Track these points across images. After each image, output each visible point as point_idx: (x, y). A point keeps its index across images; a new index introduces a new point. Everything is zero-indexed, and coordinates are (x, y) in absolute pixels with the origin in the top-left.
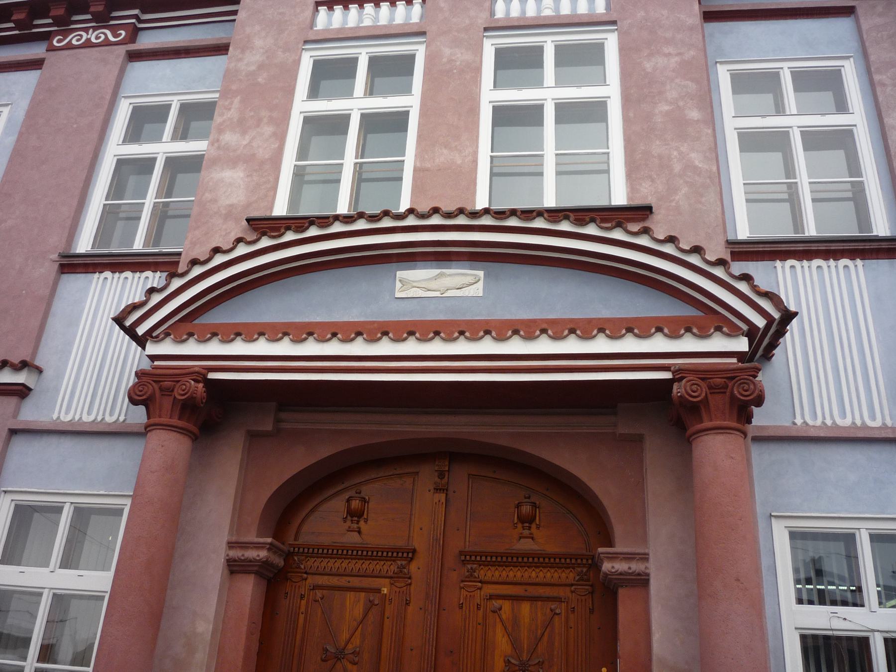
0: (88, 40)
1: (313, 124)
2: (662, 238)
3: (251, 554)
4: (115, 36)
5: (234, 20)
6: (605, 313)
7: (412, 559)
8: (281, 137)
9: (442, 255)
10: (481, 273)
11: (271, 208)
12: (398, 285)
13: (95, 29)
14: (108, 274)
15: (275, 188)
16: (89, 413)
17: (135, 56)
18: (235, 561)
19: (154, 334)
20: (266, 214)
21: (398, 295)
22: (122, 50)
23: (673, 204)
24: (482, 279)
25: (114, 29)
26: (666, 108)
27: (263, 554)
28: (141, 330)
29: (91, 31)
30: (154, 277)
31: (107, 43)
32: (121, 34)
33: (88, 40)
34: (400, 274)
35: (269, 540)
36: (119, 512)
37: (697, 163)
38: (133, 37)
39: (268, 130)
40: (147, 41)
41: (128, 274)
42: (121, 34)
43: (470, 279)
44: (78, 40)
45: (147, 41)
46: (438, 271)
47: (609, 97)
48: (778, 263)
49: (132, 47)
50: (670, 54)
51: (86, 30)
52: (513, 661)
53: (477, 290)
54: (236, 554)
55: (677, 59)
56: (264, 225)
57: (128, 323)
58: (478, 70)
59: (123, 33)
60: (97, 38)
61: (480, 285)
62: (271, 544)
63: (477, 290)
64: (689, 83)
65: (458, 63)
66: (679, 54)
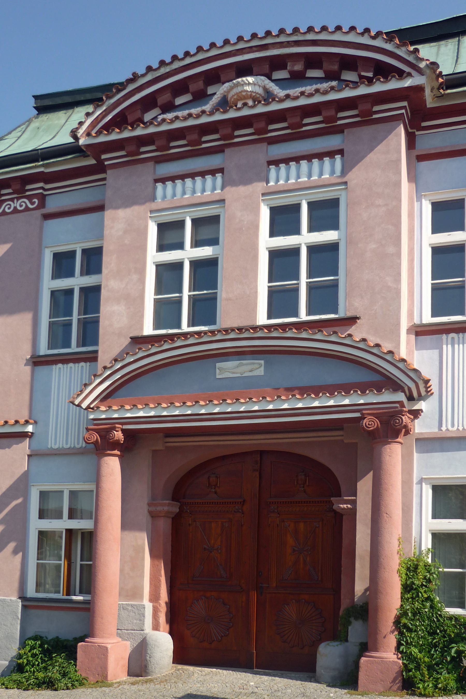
0: (15, 208)
1: (162, 268)
2: (358, 340)
3: (159, 508)
4: (32, 203)
5: (105, 184)
6: (330, 380)
7: (243, 504)
8: (142, 281)
9: (240, 354)
10: (262, 362)
11: (142, 329)
12: (218, 371)
13: (18, 199)
14: (60, 365)
15: (142, 316)
16: (55, 444)
17: (47, 217)
18: (152, 512)
19: (92, 406)
20: (140, 335)
21: (218, 377)
23: (373, 312)
24: (263, 365)
25: (30, 198)
26: (373, 246)
27: (166, 508)
28: (84, 405)
29: (15, 201)
30: (86, 366)
31: (27, 209)
32: (35, 202)
33: (15, 208)
34: (218, 365)
35: (167, 502)
36: (92, 491)
37: (390, 284)
38: (42, 205)
39: (135, 277)
40: (53, 204)
41: (71, 365)
42: (35, 202)
43: (257, 366)
44: (9, 208)
45: (53, 204)
46: (238, 362)
47: (340, 240)
48: (444, 336)
49: (44, 211)
50: (379, 206)
51: (12, 200)
52: (296, 549)
53: (261, 372)
55: (384, 209)
56: (139, 341)
57: (77, 402)
58: (257, 227)
59: (36, 200)
60: (21, 206)
61: (262, 369)
62: (169, 503)
63: (261, 372)
64: (390, 227)
65: (245, 222)
66: (386, 205)
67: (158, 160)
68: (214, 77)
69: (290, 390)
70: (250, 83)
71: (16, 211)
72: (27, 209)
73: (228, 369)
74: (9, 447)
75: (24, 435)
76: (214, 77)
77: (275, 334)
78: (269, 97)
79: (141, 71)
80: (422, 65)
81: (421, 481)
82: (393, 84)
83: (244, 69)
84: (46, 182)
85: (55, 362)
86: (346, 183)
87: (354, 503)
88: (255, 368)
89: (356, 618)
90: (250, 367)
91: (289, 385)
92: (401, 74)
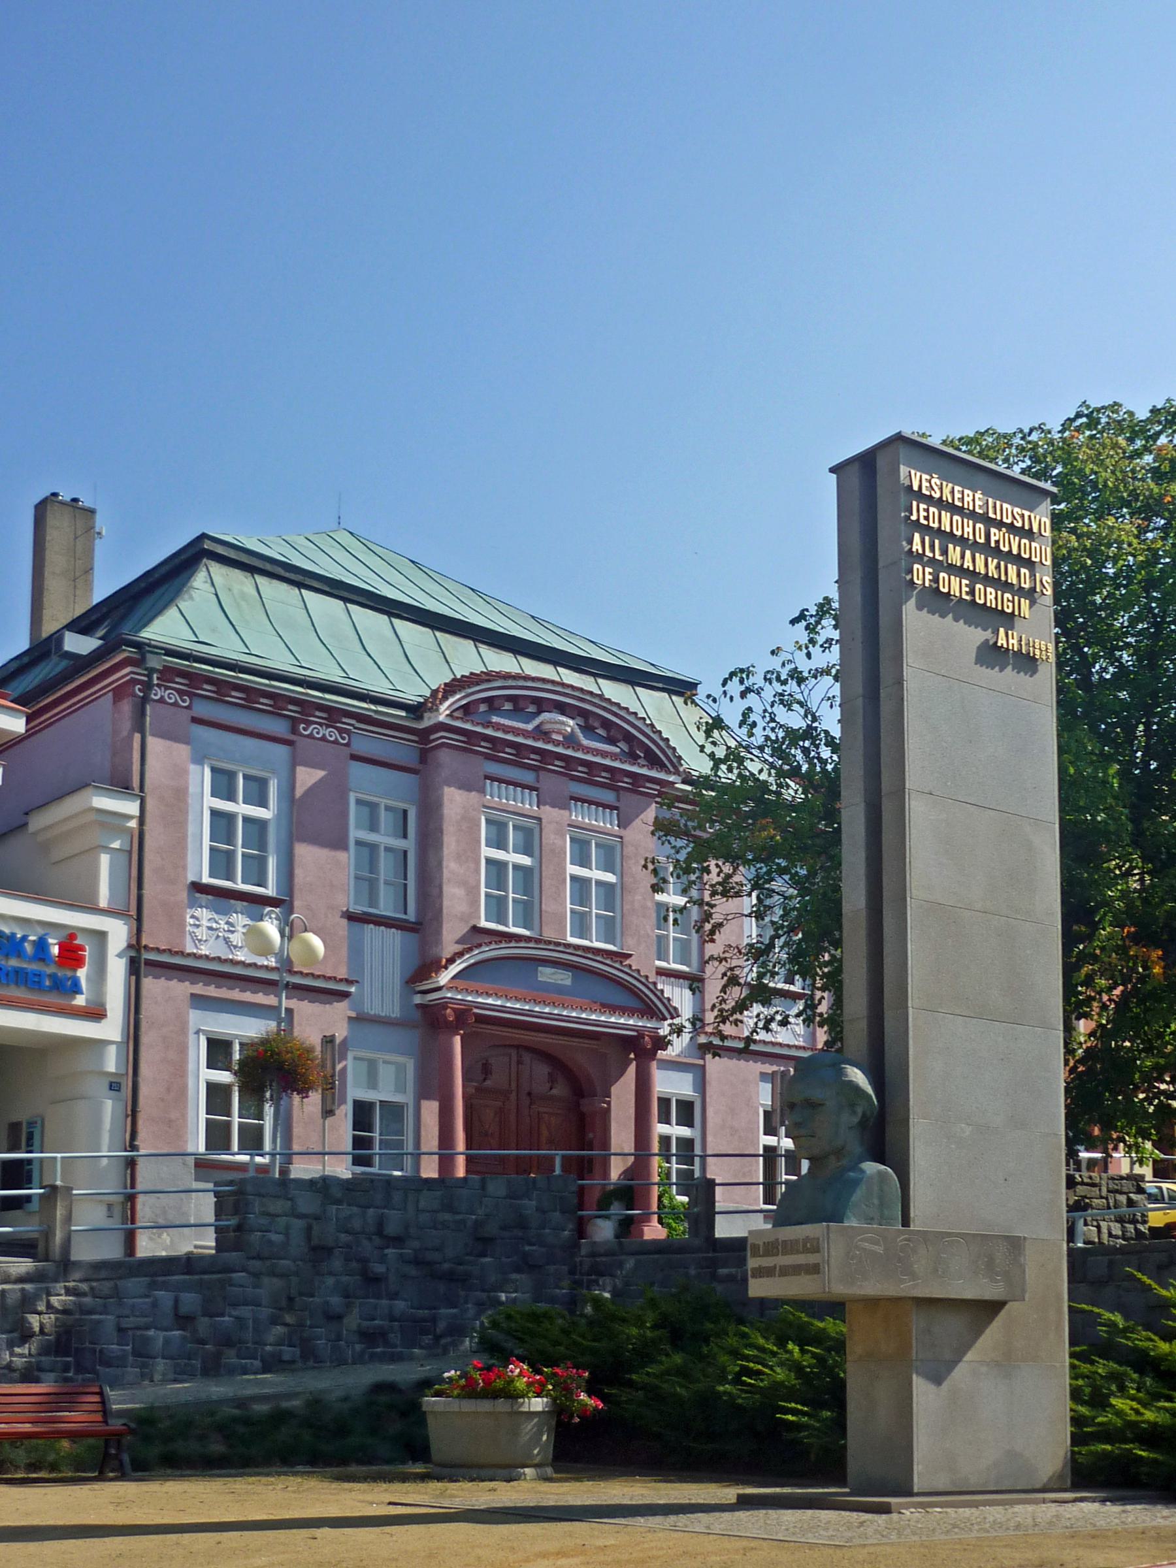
13: (328, 726)
14: (371, 926)
22: (187, 714)
34: (540, 968)
51: (321, 724)
53: (568, 982)
54: (674, 1120)
63: (568, 982)
67: (488, 757)
68: (541, 705)
69: (603, 1005)
70: (570, 724)
71: (323, 739)
72: (336, 742)
73: (547, 974)
74: (330, 1003)
75: (345, 995)
76: (541, 705)
77: (590, 956)
78: (570, 741)
79: (665, 736)
80: (681, 769)
81: (198, 1032)
82: (661, 776)
83: (562, 708)
84: (359, 721)
85: (368, 922)
86: (621, 837)
87: (609, 1103)
88: (564, 978)
89: (616, 1199)
90: (562, 977)
91: (604, 1001)
92: (668, 772)
